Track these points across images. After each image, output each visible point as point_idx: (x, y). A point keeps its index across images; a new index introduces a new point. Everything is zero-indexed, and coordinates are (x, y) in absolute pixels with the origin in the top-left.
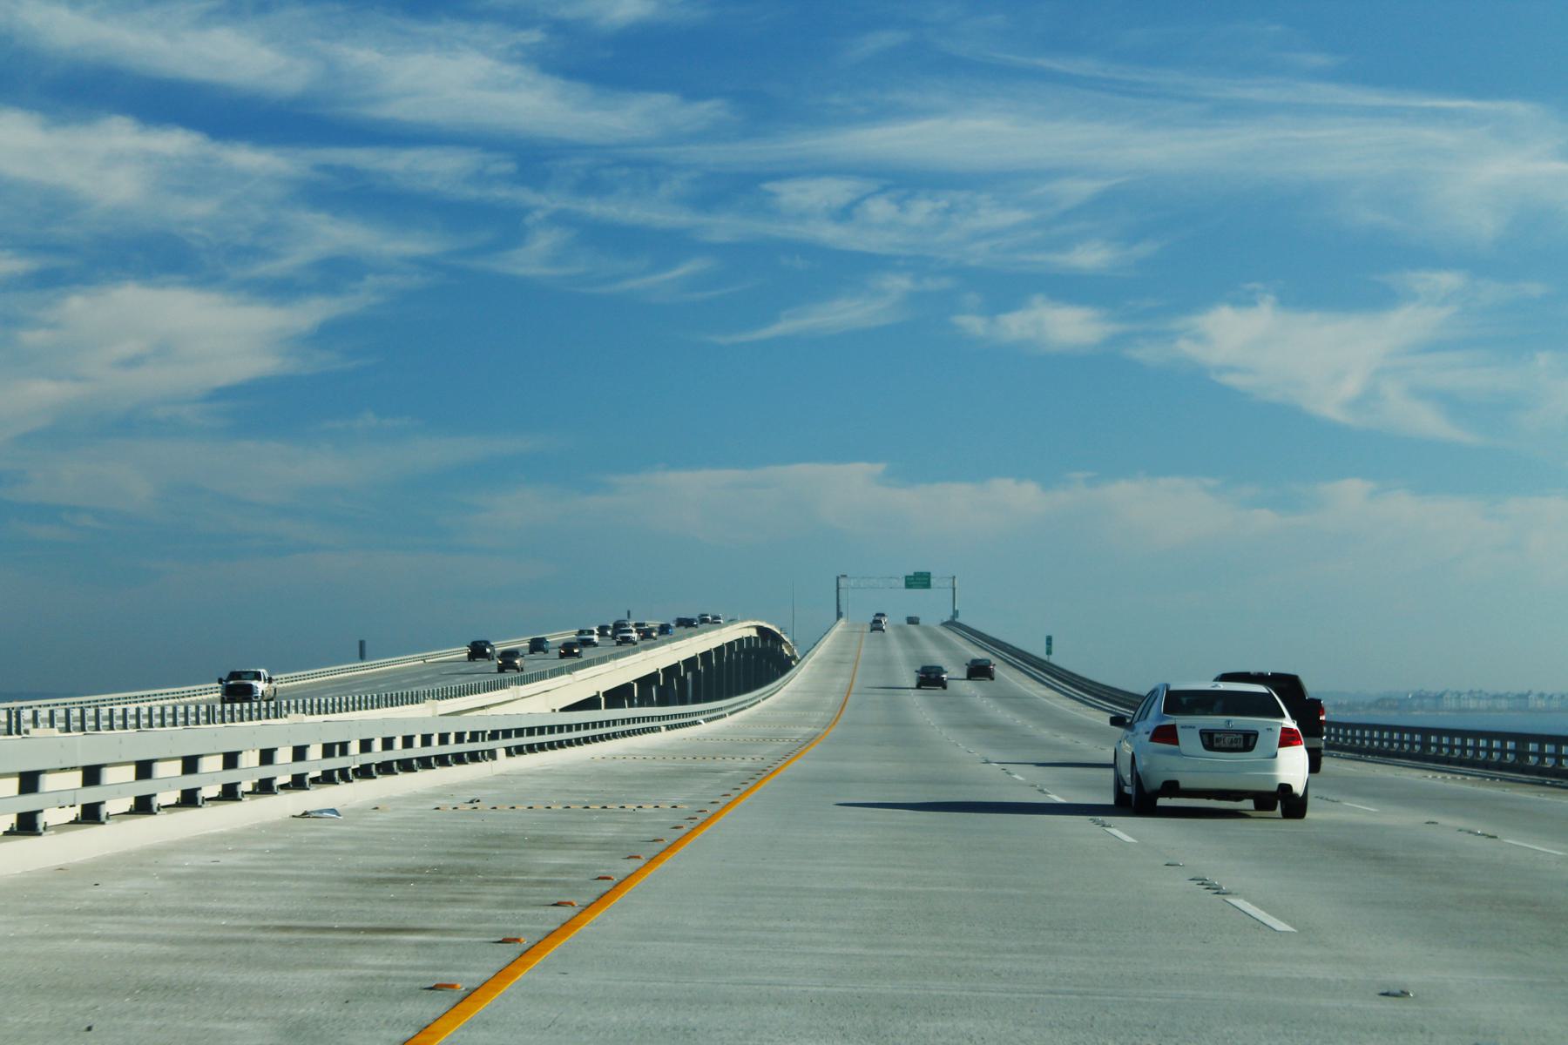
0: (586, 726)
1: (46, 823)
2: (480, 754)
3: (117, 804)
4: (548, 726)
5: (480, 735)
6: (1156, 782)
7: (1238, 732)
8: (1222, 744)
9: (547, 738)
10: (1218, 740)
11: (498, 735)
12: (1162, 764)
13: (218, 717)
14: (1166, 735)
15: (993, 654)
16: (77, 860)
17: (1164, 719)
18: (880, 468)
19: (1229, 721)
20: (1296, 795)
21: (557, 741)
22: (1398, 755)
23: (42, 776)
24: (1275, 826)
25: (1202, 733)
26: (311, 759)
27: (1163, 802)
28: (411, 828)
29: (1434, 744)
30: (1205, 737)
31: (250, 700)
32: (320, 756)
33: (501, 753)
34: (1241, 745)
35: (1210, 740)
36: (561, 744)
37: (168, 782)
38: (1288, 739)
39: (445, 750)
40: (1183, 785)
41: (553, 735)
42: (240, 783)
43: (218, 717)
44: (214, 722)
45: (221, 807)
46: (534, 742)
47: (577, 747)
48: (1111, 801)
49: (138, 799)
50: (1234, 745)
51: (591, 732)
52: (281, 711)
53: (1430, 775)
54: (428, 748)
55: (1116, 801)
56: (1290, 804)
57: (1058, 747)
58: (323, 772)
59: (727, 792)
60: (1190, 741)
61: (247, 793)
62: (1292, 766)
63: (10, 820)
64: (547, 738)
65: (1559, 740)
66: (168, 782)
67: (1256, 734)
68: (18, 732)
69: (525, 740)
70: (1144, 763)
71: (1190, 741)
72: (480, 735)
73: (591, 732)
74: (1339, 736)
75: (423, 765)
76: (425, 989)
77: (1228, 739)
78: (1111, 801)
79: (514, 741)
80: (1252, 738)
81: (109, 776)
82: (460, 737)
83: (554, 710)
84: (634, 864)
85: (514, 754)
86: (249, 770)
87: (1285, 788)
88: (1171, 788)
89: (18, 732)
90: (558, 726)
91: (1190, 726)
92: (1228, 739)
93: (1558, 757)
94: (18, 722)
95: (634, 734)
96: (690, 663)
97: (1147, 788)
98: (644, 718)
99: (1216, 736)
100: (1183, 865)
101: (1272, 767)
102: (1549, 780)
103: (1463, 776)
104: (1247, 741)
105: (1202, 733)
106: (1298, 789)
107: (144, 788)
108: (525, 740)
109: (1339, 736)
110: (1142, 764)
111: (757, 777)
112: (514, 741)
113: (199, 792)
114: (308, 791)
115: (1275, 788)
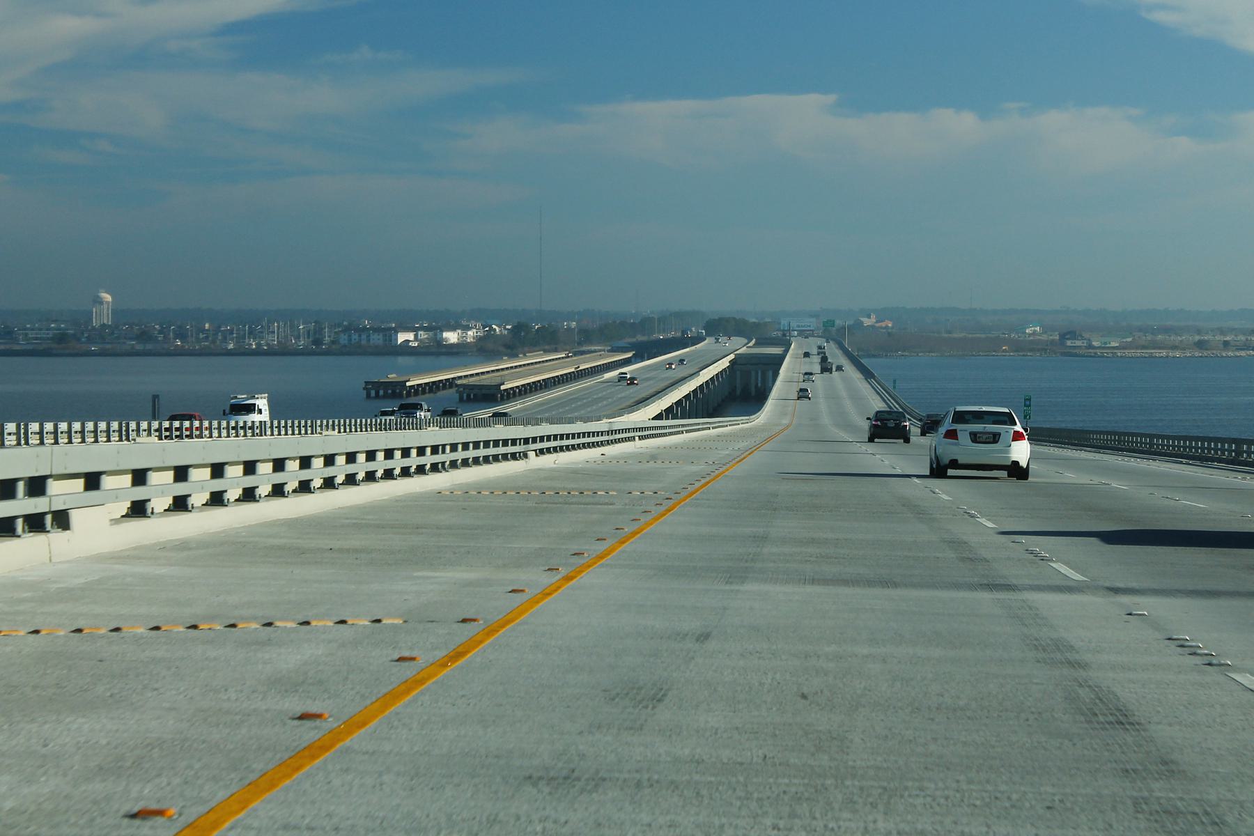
0: (562, 437)
1: (192, 504)
2: (440, 465)
3: (160, 503)
4: (484, 441)
5: (518, 441)
6: (946, 461)
7: (989, 433)
8: (981, 440)
9: (492, 451)
10: (979, 437)
11: (457, 447)
12: (951, 450)
13: (269, 432)
14: (951, 434)
15: (873, 387)
16: (107, 551)
17: (951, 426)
18: (832, 98)
19: (985, 427)
20: (1022, 467)
21: (511, 453)
22: (1213, 460)
23: (336, 457)
24: (1015, 485)
25: (971, 434)
26: (338, 464)
27: (950, 472)
28: (1027, 355)
29: (1245, 452)
30: (972, 436)
31: (505, 416)
32: (344, 463)
33: (532, 454)
34: (992, 440)
35: (975, 437)
36: (496, 458)
37: (200, 485)
38: (1018, 437)
39: (454, 456)
40: (960, 462)
41: (543, 444)
42: (226, 491)
43: (269, 432)
44: (265, 435)
45: (184, 516)
46: (563, 445)
47: (588, 449)
48: (928, 474)
49: (274, 486)
50: (988, 440)
51: (591, 440)
52: (316, 428)
53: (1052, 449)
54: (408, 459)
55: (930, 473)
56: (1017, 472)
57: (667, 378)
58: (300, 482)
59: (686, 486)
60: (964, 438)
61: (340, 484)
62: (1021, 452)
63: (124, 507)
64: (492, 451)
65: (1250, 442)
66: (201, 485)
67: (1000, 434)
68: (128, 439)
69: (546, 445)
70: (940, 451)
71: (964, 438)
72: (440, 447)
73: (591, 440)
74: (1121, 441)
75: (30, 528)
76: (510, 592)
77: (985, 437)
78: (928, 474)
79: (539, 446)
80: (997, 437)
81: (153, 478)
82: (421, 451)
83: (649, 419)
84: (555, 578)
85: (481, 463)
86: (317, 472)
87: (1016, 463)
88: (954, 464)
89: (128, 439)
90: (503, 440)
91: (964, 429)
92: (985, 437)
93: (1249, 453)
94: (127, 431)
95: (612, 443)
96: (687, 397)
97: (942, 464)
98: (594, 433)
99: (978, 435)
100: (1217, 655)
101: (1008, 452)
102: (1102, 451)
103: (1129, 458)
104: (995, 438)
105: (971, 434)
106: (1023, 464)
107: (181, 488)
108: (546, 445)
109: (1121, 441)
110: (939, 451)
111: (712, 474)
112: (539, 446)
113: (257, 490)
114: (312, 495)
115: (1010, 463)
